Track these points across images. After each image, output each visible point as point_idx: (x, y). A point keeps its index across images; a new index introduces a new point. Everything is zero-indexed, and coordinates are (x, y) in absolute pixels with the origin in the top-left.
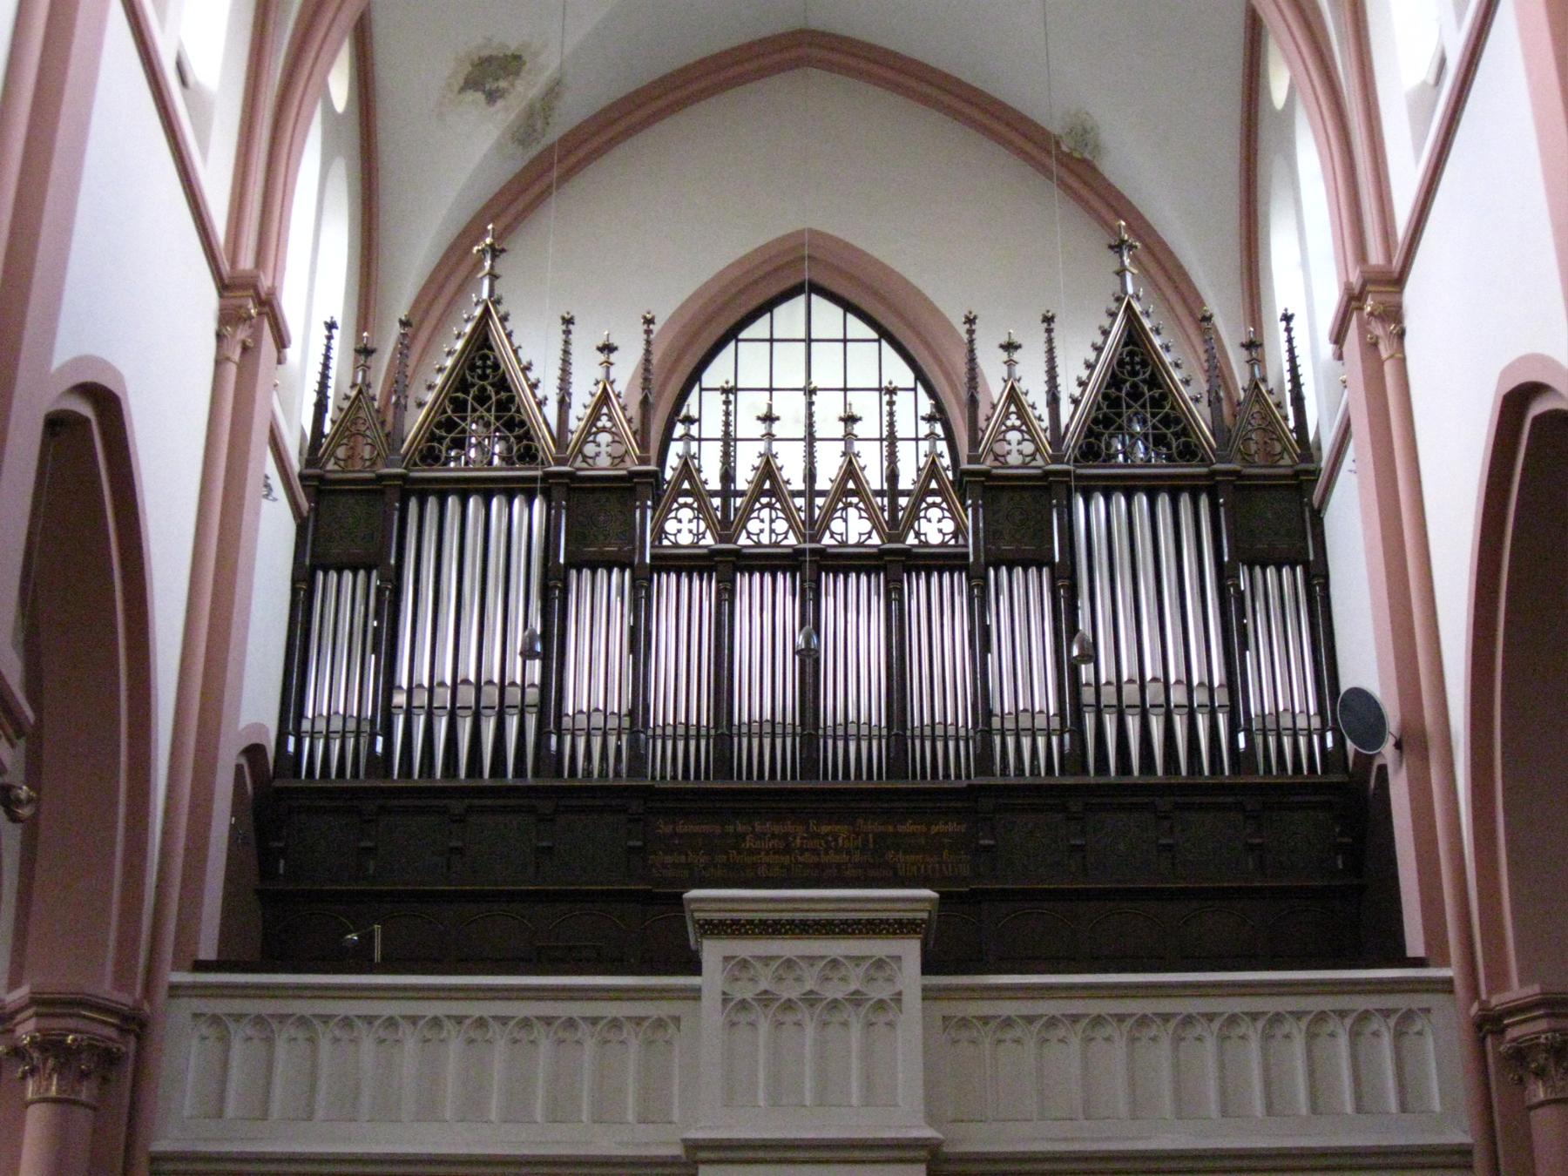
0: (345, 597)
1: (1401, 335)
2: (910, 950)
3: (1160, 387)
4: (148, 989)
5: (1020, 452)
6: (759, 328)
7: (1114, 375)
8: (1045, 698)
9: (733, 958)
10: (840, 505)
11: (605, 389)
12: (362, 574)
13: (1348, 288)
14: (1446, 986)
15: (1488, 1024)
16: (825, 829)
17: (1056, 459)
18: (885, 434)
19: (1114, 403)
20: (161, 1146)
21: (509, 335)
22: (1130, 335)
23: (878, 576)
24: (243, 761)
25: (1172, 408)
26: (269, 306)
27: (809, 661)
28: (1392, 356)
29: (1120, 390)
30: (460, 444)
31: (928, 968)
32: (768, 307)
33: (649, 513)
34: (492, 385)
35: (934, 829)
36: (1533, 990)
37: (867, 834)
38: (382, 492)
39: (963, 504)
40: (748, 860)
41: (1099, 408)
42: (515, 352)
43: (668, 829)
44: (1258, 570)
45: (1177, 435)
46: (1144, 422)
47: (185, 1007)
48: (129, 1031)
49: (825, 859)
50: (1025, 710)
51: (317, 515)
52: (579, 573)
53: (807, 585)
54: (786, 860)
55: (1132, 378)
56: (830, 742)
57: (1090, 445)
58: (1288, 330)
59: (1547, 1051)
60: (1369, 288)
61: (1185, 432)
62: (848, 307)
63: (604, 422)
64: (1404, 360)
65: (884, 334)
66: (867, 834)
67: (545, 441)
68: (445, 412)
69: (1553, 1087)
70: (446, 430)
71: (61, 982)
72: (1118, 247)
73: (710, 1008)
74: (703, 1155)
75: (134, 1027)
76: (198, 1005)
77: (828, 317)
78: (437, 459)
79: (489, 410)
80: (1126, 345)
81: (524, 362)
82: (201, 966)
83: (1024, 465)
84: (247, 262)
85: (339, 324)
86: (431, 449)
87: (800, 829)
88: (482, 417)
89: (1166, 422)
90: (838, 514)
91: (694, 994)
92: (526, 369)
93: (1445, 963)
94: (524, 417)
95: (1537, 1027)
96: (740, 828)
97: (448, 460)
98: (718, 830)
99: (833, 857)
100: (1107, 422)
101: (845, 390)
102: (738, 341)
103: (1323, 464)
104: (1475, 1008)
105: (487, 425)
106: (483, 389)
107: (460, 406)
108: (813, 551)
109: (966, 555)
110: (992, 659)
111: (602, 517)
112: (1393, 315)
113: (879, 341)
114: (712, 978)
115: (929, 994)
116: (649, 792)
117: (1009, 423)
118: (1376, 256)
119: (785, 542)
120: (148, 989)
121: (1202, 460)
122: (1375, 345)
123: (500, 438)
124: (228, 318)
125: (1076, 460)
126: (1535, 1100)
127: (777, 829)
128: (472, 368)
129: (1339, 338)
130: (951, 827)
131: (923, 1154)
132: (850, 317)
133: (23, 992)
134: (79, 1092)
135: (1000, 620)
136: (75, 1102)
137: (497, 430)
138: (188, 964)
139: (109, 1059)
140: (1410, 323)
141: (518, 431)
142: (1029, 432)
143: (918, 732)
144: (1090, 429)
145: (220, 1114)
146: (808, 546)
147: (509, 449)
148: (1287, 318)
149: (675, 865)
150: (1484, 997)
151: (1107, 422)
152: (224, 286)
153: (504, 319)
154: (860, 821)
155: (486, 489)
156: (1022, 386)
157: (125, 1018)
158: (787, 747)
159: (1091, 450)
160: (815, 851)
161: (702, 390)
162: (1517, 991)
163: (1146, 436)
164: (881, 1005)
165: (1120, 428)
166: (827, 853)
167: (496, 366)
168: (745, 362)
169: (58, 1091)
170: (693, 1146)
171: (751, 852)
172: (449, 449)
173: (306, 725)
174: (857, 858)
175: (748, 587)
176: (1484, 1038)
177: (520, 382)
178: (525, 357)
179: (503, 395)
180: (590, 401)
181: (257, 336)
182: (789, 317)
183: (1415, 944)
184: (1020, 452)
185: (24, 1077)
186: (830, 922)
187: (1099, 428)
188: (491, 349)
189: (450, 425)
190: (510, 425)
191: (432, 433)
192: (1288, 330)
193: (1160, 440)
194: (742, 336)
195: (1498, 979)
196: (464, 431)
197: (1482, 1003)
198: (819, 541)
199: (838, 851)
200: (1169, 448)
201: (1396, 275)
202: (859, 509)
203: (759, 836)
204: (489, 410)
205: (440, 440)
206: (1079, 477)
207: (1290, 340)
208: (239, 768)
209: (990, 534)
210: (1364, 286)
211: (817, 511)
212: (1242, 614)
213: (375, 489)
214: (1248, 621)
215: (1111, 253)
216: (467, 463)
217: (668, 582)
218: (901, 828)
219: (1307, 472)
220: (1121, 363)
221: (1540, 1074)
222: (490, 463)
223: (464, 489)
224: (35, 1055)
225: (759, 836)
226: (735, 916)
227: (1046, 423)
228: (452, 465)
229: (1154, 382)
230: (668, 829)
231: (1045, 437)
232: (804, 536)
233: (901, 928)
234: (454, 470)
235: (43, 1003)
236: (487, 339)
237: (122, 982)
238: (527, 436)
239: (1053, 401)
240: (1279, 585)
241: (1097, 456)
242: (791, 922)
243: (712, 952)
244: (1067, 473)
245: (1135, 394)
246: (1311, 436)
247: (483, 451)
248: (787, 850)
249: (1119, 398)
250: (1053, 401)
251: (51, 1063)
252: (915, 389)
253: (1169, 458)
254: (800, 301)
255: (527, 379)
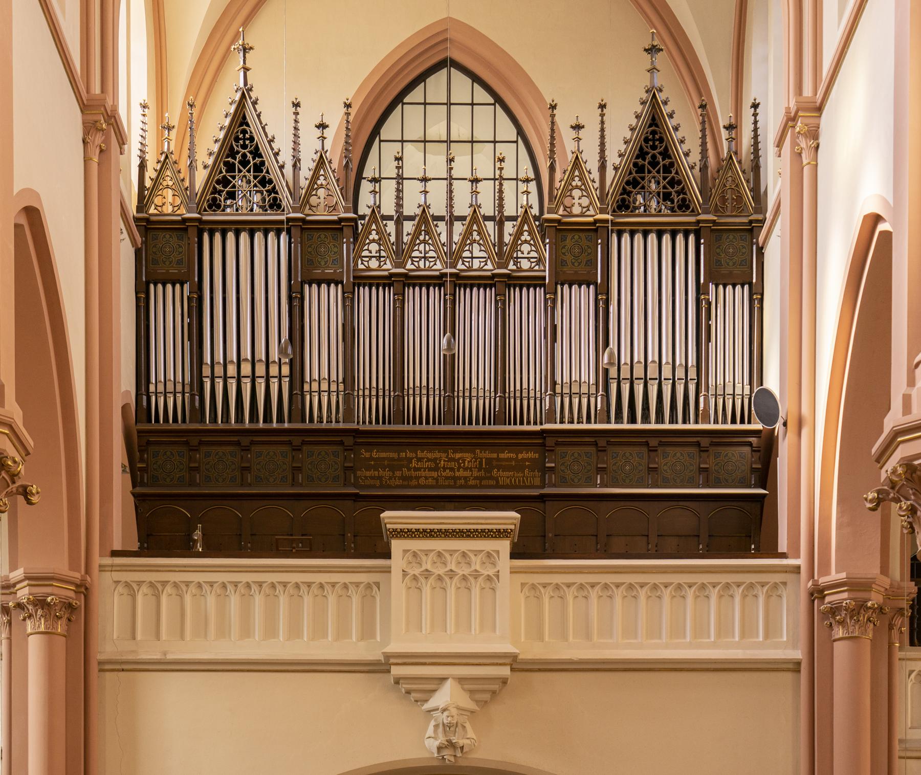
0: (169, 304)
1: (817, 148)
2: (504, 546)
3: (670, 157)
4: (88, 571)
5: (580, 205)
6: (416, 95)
7: (641, 149)
8: (587, 375)
9: (409, 551)
10: (468, 242)
11: (321, 155)
12: (178, 286)
13: (788, 110)
14: (797, 569)
15: (817, 593)
16: (458, 456)
17: (602, 211)
18: (497, 177)
19: (640, 169)
20: (101, 657)
21: (259, 116)
22: (653, 119)
23: (491, 289)
24: (23, 221)
25: (677, 173)
26: (112, 119)
27: (450, 363)
28: (809, 163)
29: (644, 160)
30: (232, 195)
31: (514, 555)
32: (421, 78)
33: (352, 246)
34: (250, 152)
35: (520, 456)
36: (843, 575)
37: (481, 459)
38: (186, 230)
39: (543, 242)
40: (413, 473)
41: (630, 173)
42: (263, 128)
43: (367, 455)
44: (721, 287)
45: (678, 193)
46: (658, 183)
47: (108, 578)
48: (80, 592)
49: (457, 474)
50: (576, 381)
51: (146, 246)
52: (310, 286)
53: (448, 297)
54: (435, 474)
55: (652, 148)
56: (461, 400)
57: (623, 200)
58: (755, 115)
59: (846, 610)
60: (800, 114)
61: (682, 191)
62: (475, 78)
63: (321, 181)
64: (816, 165)
65: (498, 100)
66: (481, 459)
67: (282, 181)
68: (221, 172)
69: (848, 630)
70: (221, 187)
71: (41, 567)
72: (652, 50)
73: (397, 584)
74: (392, 661)
75: (83, 590)
76: (117, 576)
77: (462, 87)
78: (219, 206)
79: (249, 171)
80: (650, 126)
81: (270, 137)
82: (115, 554)
83: (582, 215)
84: (96, 89)
85: (150, 105)
86: (214, 199)
87: (444, 455)
88: (245, 176)
89: (672, 183)
90: (467, 248)
91: (387, 570)
92: (270, 141)
93: (798, 557)
94: (272, 177)
95: (842, 597)
96: (409, 455)
97: (226, 207)
98: (395, 455)
99: (461, 473)
100: (634, 183)
101: (472, 104)
102: (404, 104)
103: (768, 215)
104: (810, 583)
105: (249, 182)
106: (244, 156)
107: (230, 168)
108: (452, 275)
109: (544, 278)
110: (558, 345)
111: (320, 245)
112: (814, 134)
113: (494, 104)
114: (397, 561)
115: (513, 571)
116: (356, 433)
117: (574, 184)
118: (807, 91)
119: (435, 267)
120: (88, 571)
121: (693, 211)
122: (800, 154)
123: (257, 192)
124: (90, 128)
125: (614, 211)
126: (837, 637)
127: (430, 455)
128: (237, 139)
129: (779, 144)
130: (531, 455)
131: (508, 661)
132: (475, 84)
133: (19, 574)
134: (57, 628)
135: (562, 317)
136: (54, 633)
137: (255, 186)
138: (108, 553)
139: (70, 607)
140: (822, 140)
141: (269, 187)
142: (586, 190)
143: (512, 395)
144: (624, 189)
145: (134, 638)
146: (449, 271)
147: (264, 200)
148: (755, 106)
149: (372, 478)
150: (816, 578)
151: (634, 183)
152: (84, 107)
153: (255, 103)
154: (478, 451)
155: (252, 228)
156: (584, 156)
157: (77, 586)
158: (435, 401)
159: (623, 205)
160: (452, 469)
161: (380, 141)
162: (835, 575)
163: (659, 194)
164: (489, 578)
165: (643, 187)
166: (458, 471)
167: (252, 139)
168: (409, 120)
169: (46, 627)
170: (388, 656)
171: (416, 469)
172: (226, 199)
173: (152, 388)
174: (476, 474)
175: (413, 296)
176: (813, 601)
177: (264, 149)
178: (270, 132)
179: (258, 160)
180: (313, 165)
181: (107, 141)
182: (436, 86)
183: (783, 546)
184: (580, 205)
185: (24, 620)
186: (461, 531)
187: (629, 188)
188: (248, 125)
189: (225, 182)
190: (264, 182)
191: (215, 188)
192: (755, 115)
193: (667, 197)
194: (405, 101)
195: (825, 570)
196: (234, 186)
197: (814, 581)
198: (455, 267)
199: (465, 469)
200: (673, 202)
201: (818, 104)
202: (480, 244)
203: (420, 460)
204: (249, 171)
205: (220, 192)
206: (614, 224)
207: (756, 122)
208: (17, 226)
209: (557, 263)
210: (797, 112)
211: (454, 246)
212: (709, 317)
213: (181, 227)
214: (712, 322)
215: (645, 53)
216: (237, 210)
217: (364, 292)
218: (502, 456)
219: (758, 221)
220: (646, 140)
221: (842, 623)
222: (252, 210)
223: (238, 227)
224: (30, 607)
225: (420, 460)
226: (410, 527)
227: (597, 185)
228: (228, 210)
229: (666, 154)
230: (367, 455)
231: (595, 194)
232: (446, 263)
233: (499, 534)
234: (229, 215)
235: (33, 579)
236: (244, 117)
237: (73, 566)
238: (274, 190)
239: (602, 168)
240: (731, 301)
241: (627, 207)
242: (440, 531)
243: (397, 546)
244: (606, 221)
245: (654, 164)
246: (762, 190)
247: (247, 203)
248: (436, 469)
249: (643, 166)
250: (602, 168)
251: (40, 612)
252: (516, 142)
253: (672, 210)
254: (445, 71)
255: (272, 149)
